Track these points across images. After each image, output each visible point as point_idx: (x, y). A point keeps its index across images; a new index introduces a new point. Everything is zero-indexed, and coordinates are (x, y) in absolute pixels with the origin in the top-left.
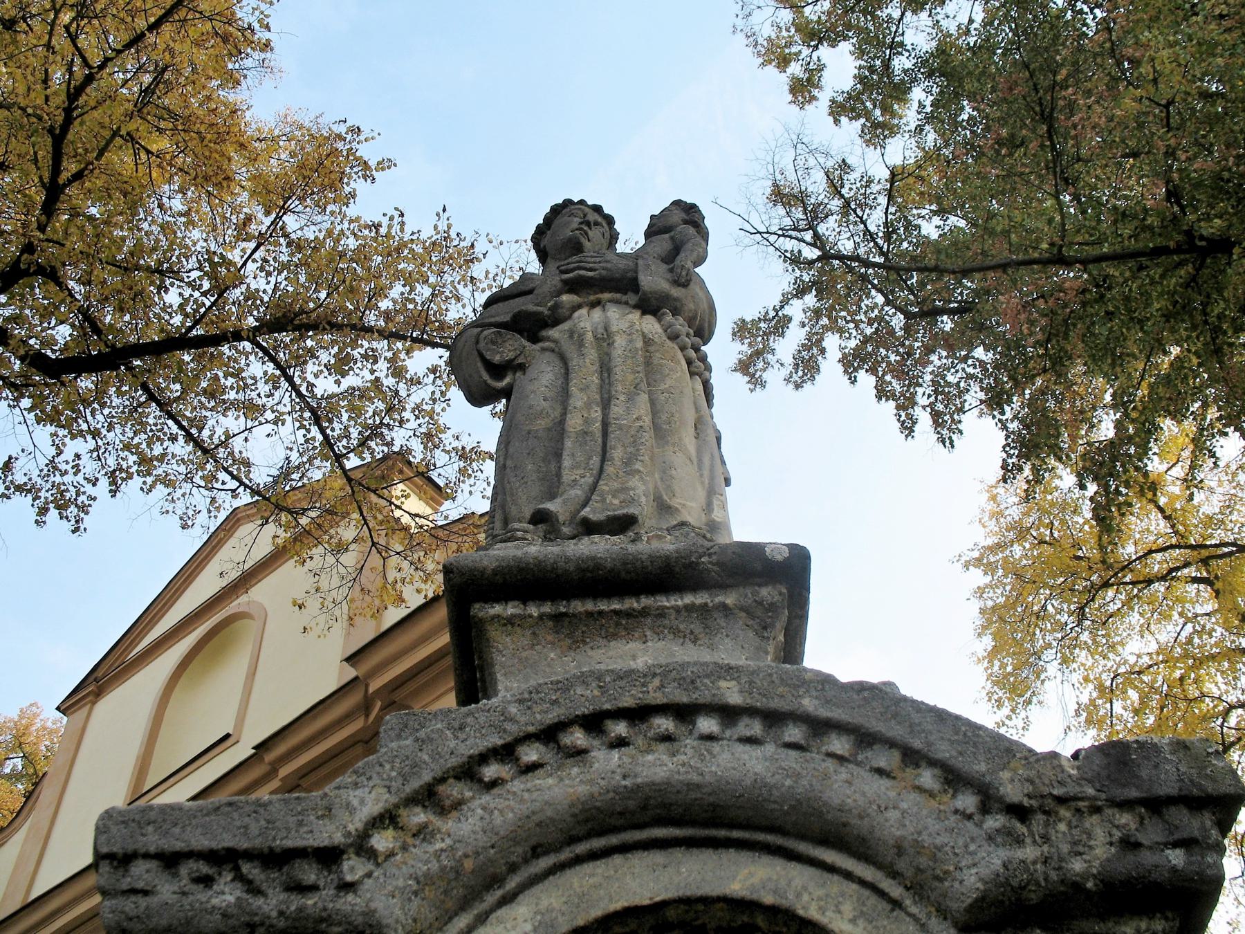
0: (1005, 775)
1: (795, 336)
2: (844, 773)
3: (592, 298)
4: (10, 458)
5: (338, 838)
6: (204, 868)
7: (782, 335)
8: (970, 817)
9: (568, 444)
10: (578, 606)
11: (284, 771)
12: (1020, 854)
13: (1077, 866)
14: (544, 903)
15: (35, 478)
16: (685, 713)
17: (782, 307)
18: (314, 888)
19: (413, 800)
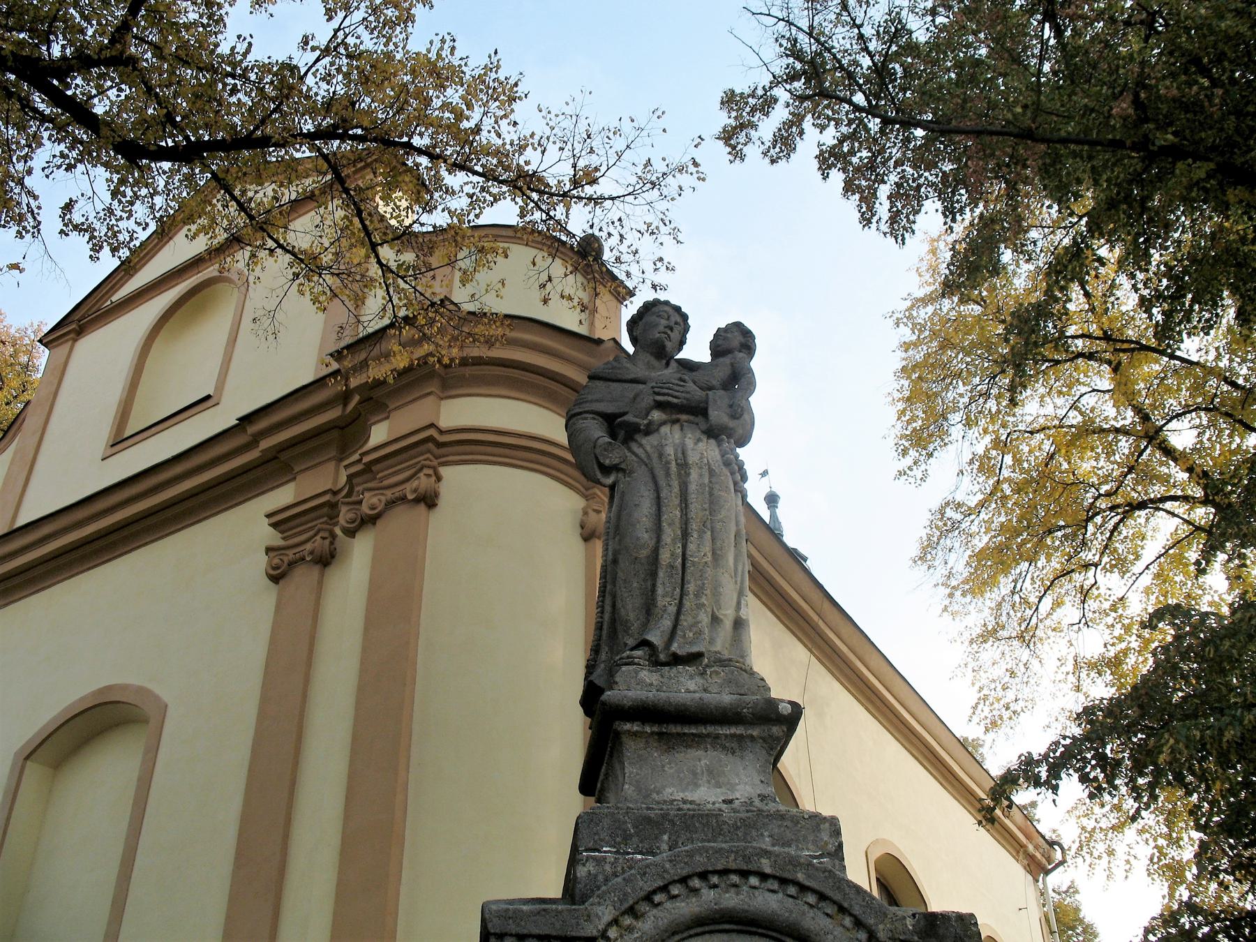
0: (881, 927)
1: (780, 114)
2: (811, 913)
3: (674, 417)
4: (71, 200)
5: (595, 933)
7: (767, 114)
9: (661, 574)
10: (674, 729)
11: (265, 444)
16: (745, 874)
17: (771, 88)
19: (623, 914)
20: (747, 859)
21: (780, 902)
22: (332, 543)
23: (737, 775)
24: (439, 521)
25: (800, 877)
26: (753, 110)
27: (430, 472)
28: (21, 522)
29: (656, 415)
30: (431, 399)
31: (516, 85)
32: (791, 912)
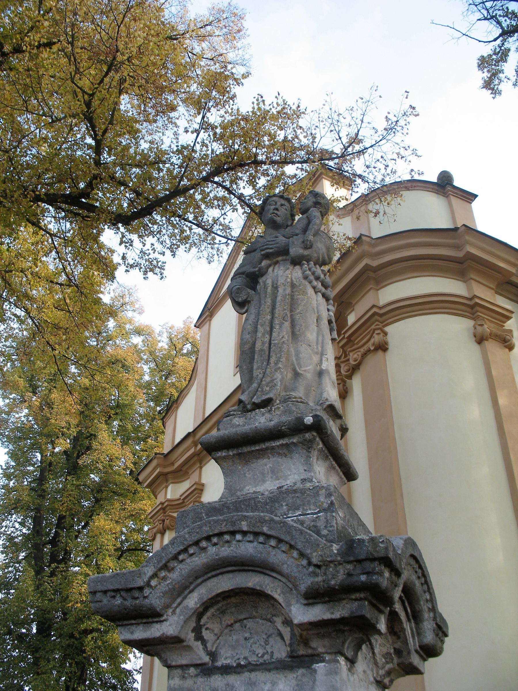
0: (314, 554)
3: (275, 260)
5: (142, 584)
6: (113, 594)
7: (506, 61)
8: (305, 567)
10: (246, 449)
12: (316, 579)
13: (333, 582)
14: (201, 592)
15: (137, 260)
16: (233, 533)
17: (503, 44)
18: (138, 598)
19: (161, 569)
20: (233, 523)
21: (255, 548)
22: (344, 385)
23: (289, 469)
24: (392, 358)
25: (265, 529)
26: (498, 61)
27: (379, 331)
28: (207, 415)
29: (264, 263)
30: (371, 293)
31: (299, 107)
32: (261, 553)
